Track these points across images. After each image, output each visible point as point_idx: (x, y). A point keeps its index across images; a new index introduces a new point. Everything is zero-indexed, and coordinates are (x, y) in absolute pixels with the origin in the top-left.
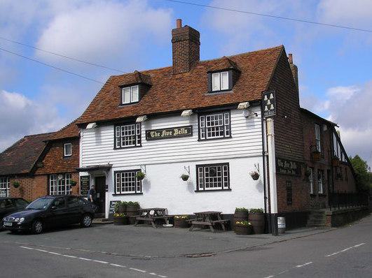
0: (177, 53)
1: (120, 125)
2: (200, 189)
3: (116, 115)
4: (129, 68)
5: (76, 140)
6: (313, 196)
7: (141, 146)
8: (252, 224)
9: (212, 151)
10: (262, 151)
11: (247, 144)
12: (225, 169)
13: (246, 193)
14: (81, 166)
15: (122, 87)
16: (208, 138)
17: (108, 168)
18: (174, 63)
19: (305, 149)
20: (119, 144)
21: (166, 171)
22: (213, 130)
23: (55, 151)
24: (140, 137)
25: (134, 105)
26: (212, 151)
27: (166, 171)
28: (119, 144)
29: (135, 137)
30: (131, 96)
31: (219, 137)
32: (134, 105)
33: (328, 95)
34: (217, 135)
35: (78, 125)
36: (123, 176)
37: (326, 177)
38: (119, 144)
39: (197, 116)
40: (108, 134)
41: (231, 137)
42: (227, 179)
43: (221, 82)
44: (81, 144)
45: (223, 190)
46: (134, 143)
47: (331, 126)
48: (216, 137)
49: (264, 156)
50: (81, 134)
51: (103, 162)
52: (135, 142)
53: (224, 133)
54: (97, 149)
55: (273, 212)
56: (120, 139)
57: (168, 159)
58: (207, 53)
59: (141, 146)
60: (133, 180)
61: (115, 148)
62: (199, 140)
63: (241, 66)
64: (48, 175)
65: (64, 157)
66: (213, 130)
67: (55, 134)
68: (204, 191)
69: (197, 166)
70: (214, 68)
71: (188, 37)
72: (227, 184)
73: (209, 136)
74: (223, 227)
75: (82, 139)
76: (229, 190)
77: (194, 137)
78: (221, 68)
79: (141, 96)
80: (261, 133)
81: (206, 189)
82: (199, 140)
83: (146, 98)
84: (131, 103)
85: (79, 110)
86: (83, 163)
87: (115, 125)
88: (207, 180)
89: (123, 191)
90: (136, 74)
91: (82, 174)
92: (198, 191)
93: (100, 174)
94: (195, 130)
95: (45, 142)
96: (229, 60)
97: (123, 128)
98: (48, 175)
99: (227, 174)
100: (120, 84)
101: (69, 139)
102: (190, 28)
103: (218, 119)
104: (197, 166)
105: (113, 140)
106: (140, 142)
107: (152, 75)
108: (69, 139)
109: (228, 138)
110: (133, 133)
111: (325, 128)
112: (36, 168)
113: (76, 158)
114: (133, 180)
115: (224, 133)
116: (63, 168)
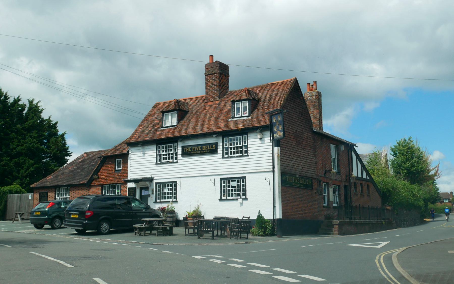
0: (209, 84)
1: (161, 144)
3: (160, 135)
4: (170, 98)
5: (125, 157)
7: (248, 155)
8: (264, 228)
9: (233, 167)
10: (272, 167)
12: (243, 182)
13: (262, 200)
15: (163, 112)
16: (230, 156)
18: (207, 93)
20: (160, 161)
21: (195, 185)
22: (234, 149)
24: (176, 154)
25: (180, 128)
26: (233, 167)
27: (195, 185)
28: (160, 161)
29: (241, 147)
30: (171, 120)
32: (180, 128)
35: (127, 143)
38: (160, 160)
39: (155, 146)
40: (151, 153)
43: (242, 112)
44: (129, 161)
46: (241, 152)
50: (130, 151)
52: (173, 158)
53: (243, 152)
54: (142, 164)
55: (6, 179)
56: (160, 156)
57: (202, 173)
58: (234, 84)
59: (248, 155)
61: (157, 164)
62: (223, 157)
64: (102, 186)
65: (116, 170)
66: (234, 149)
67: (108, 151)
69: (221, 179)
71: (217, 71)
73: (231, 154)
75: (130, 156)
77: (219, 155)
79: (180, 119)
80: (271, 152)
81: (162, 200)
82: (223, 157)
83: (183, 122)
85: (127, 132)
86: (130, 176)
87: (157, 144)
88: (229, 191)
89: (163, 199)
90: (175, 102)
92: (221, 200)
93: (145, 183)
95: (100, 157)
97: (163, 147)
98: (102, 186)
100: (163, 110)
101: (117, 157)
104: (221, 179)
105: (155, 156)
106: (176, 158)
107: (189, 102)
108: (117, 157)
109: (246, 156)
110: (240, 144)
112: (91, 180)
113: (125, 172)
115: (243, 152)
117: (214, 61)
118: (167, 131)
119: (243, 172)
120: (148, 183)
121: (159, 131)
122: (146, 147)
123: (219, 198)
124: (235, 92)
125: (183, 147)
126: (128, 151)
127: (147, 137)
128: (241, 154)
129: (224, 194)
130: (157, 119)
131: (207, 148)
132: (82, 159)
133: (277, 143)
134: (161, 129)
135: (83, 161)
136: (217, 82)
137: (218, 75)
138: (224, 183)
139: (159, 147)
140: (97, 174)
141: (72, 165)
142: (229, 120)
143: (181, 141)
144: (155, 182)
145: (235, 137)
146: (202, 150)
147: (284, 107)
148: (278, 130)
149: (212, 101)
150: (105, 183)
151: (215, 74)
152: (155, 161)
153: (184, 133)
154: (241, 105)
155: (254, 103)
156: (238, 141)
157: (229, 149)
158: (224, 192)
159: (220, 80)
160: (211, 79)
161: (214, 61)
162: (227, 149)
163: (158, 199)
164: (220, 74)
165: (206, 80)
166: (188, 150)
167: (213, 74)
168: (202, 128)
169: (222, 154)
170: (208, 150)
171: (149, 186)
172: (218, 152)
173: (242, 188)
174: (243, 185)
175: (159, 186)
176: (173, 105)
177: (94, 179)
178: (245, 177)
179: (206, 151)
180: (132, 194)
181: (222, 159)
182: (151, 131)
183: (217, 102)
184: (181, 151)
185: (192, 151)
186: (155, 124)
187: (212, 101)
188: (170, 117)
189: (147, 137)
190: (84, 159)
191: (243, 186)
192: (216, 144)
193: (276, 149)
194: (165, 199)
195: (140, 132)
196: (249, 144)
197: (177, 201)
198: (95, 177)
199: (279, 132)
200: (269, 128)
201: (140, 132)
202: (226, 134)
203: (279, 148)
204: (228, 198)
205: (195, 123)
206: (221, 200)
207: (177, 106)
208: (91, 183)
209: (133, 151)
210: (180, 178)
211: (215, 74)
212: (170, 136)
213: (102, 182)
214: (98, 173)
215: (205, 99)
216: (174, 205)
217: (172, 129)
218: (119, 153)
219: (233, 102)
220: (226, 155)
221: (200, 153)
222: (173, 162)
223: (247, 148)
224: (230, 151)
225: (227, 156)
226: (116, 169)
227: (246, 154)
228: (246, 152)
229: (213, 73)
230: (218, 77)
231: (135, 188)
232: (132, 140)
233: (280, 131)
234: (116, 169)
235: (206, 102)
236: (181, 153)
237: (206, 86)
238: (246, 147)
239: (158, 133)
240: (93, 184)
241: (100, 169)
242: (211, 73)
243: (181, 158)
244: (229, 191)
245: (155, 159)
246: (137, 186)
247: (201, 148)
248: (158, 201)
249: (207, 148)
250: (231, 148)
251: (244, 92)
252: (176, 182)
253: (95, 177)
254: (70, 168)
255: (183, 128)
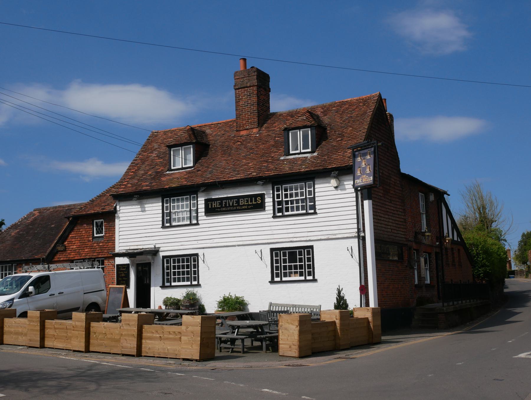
2: (277, 279)
5: (110, 216)
6: (419, 287)
9: (291, 231)
10: (356, 230)
11: (336, 223)
12: (194, 261)
14: (117, 250)
15: (170, 147)
17: (155, 252)
18: (238, 116)
19: (407, 219)
23: (82, 230)
26: (291, 231)
27: (232, 259)
28: (167, 222)
30: (183, 160)
31: (301, 212)
33: (432, 141)
34: (298, 209)
36: (174, 262)
37: (434, 262)
38: (169, 221)
39: (270, 187)
40: (154, 208)
41: (315, 213)
42: (311, 267)
43: (300, 148)
45: (306, 281)
47: (440, 195)
48: (290, 213)
49: (359, 237)
50: (118, 207)
51: (148, 244)
53: (310, 208)
54: (137, 227)
60: (185, 267)
61: (163, 227)
62: (275, 217)
63: (326, 120)
65: (94, 238)
68: (281, 282)
69: (272, 250)
70: (292, 122)
71: (255, 82)
72: (312, 273)
74: (197, 307)
76: (314, 280)
78: (299, 124)
79: (196, 160)
80: (355, 208)
81: (284, 279)
82: (275, 217)
84: (183, 168)
86: (118, 249)
89: (175, 281)
91: (119, 261)
92: (272, 282)
93: (144, 262)
94: (269, 201)
96: (311, 113)
99: (311, 259)
101: (103, 216)
102: (258, 71)
103: (296, 191)
104: (272, 250)
105: (161, 215)
107: (208, 131)
111: (432, 198)
113: (111, 239)
114: (185, 267)
115: (310, 208)
116: (94, 252)
117: (248, 67)
118: (177, 176)
119: (308, 239)
120: (150, 257)
121: (165, 176)
122: (145, 201)
123: (270, 280)
124: (281, 115)
125: (207, 201)
126: (115, 208)
127: (147, 186)
128: (304, 212)
129: (168, 279)
130: (157, 156)
131: (248, 202)
132: (31, 219)
133: (364, 192)
134: (168, 172)
135: (33, 223)
136: (255, 99)
137: (255, 88)
138: (167, 263)
139: (167, 200)
140: (63, 243)
141: (16, 228)
142: (282, 158)
143: (203, 191)
144: (162, 254)
145: (299, 184)
146: (239, 205)
147: (368, 137)
148: (363, 172)
149: (247, 129)
150: (76, 258)
151: (250, 86)
152: (161, 223)
153: (209, 178)
154: (300, 134)
155: (321, 134)
156: (299, 191)
157: (284, 203)
158: (168, 275)
159: (258, 97)
160: (244, 95)
161: (248, 67)
162: (280, 203)
163: (168, 282)
164: (259, 87)
165: (236, 97)
166: (215, 205)
167: (247, 87)
168: (238, 171)
169: (272, 212)
170: (248, 205)
171: (152, 262)
172: (267, 208)
173: (172, 271)
174: (195, 265)
175: (277, 255)
176: (186, 135)
177: (58, 251)
178: (312, 247)
179: (246, 207)
180: (123, 275)
181: (272, 220)
182: (150, 175)
183: (255, 130)
184: (203, 206)
185: (222, 207)
186: (157, 164)
187: (247, 129)
188: (181, 152)
189: (147, 186)
190: (36, 219)
191: (309, 260)
192: (262, 196)
193: (366, 203)
194: (179, 281)
195: (133, 178)
196: (316, 195)
197: (198, 285)
198: (60, 248)
199: (364, 176)
200: (345, 171)
201: (133, 178)
202: (277, 181)
203: (371, 201)
204: (284, 279)
205: (224, 162)
206: (272, 282)
207: (192, 136)
208: (53, 258)
209: (123, 206)
210: (203, 248)
211: (250, 86)
212: (185, 183)
213: (72, 256)
214: (65, 241)
215: (237, 125)
216: (195, 290)
217: (186, 172)
218: (98, 210)
219: (287, 130)
220: (281, 210)
221: (237, 210)
222: (307, 214)
223: (315, 202)
224: (285, 206)
225: (280, 214)
226: (95, 235)
227: (312, 211)
228: (313, 207)
229: (248, 85)
230: (255, 92)
231: (128, 265)
232: (121, 191)
233: (367, 174)
234: (95, 235)
235: (237, 131)
236: (203, 210)
237: (237, 106)
238: (313, 200)
239: (163, 179)
240: (56, 260)
241: (68, 236)
242: (245, 85)
243: (205, 218)
244: (174, 275)
245: (161, 219)
246: (132, 262)
247: (238, 202)
248: (167, 284)
249: (248, 202)
250: (287, 203)
251: (302, 115)
252: (197, 255)
253: (60, 248)
254: (13, 234)
255: (205, 171)
